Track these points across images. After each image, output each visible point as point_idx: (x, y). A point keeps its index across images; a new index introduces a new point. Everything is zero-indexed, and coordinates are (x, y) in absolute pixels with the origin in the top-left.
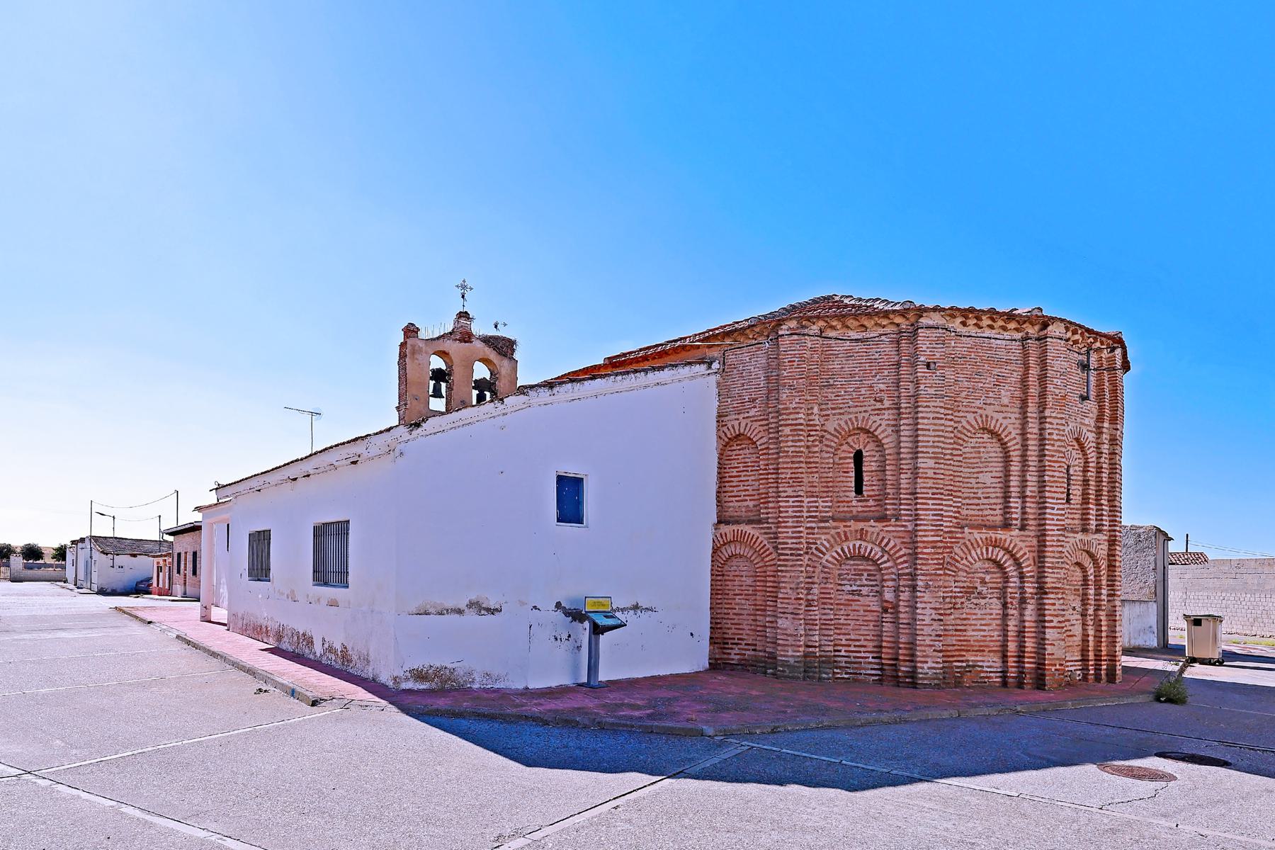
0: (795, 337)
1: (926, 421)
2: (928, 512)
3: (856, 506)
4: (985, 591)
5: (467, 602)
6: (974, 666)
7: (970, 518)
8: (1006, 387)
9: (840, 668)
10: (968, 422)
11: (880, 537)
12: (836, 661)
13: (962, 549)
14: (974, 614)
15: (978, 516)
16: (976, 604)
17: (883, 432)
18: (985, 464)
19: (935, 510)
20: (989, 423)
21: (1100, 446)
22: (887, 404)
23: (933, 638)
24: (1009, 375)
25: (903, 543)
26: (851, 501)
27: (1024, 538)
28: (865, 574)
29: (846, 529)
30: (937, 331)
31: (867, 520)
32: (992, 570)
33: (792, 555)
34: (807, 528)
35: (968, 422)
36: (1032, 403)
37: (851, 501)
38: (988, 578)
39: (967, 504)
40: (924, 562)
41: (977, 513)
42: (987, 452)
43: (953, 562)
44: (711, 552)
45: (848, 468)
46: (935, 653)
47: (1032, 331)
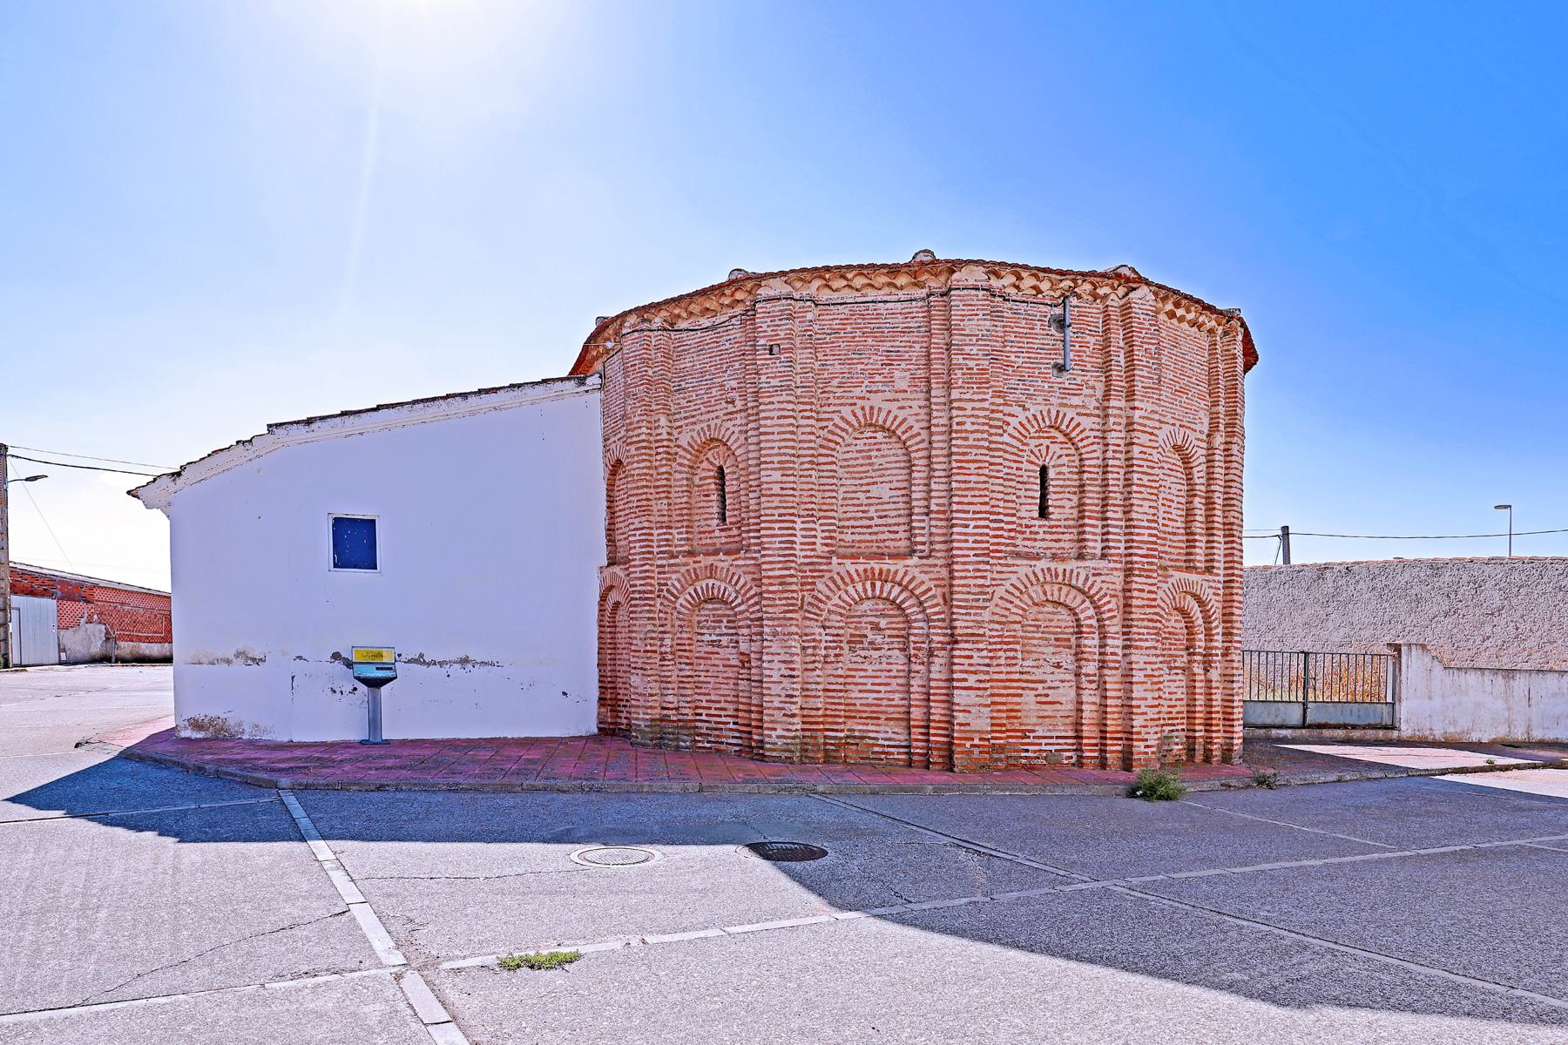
0: (636, 334)
1: (769, 422)
2: (774, 539)
3: (720, 538)
4: (879, 639)
5: (234, 652)
6: (862, 738)
7: (857, 545)
8: (903, 366)
9: (701, 735)
10: (842, 418)
11: (730, 573)
12: (697, 727)
13: (827, 586)
14: (862, 670)
15: (872, 541)
16: (865, 658)
17: (735, 441)
18: (879, 473)
19: (782, 535)
20: (875, 416)
21: (1106, 435)
22: (739, 405)
23: (783, 699)
24: (907, 349)
25: (754, 579)
26: (714, 531)
27: (926, 569)
28: (725, 620)
29: (696, 565)
30: (780, 303)
31: (716, 553)
32: (891, 612)
33: (640, 599)
34: (658, 566)
35: (842, 418)
36: (937, 383)
37: (714, 531)
38: (883, 623)
39: (853, 527)
40: (771, 603)
41: (868, 537)
42: (883, 456)
43: (816, 602)
44: (598, 599)
45: (708, 490)
46: (785, 719)
47: (935, 284)
